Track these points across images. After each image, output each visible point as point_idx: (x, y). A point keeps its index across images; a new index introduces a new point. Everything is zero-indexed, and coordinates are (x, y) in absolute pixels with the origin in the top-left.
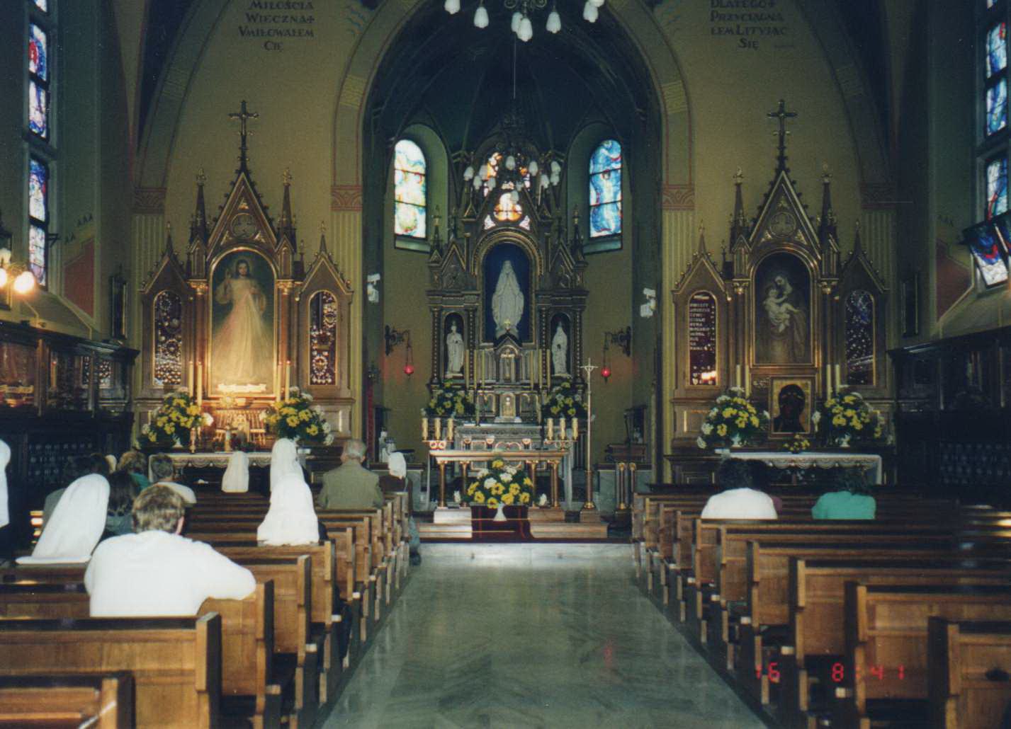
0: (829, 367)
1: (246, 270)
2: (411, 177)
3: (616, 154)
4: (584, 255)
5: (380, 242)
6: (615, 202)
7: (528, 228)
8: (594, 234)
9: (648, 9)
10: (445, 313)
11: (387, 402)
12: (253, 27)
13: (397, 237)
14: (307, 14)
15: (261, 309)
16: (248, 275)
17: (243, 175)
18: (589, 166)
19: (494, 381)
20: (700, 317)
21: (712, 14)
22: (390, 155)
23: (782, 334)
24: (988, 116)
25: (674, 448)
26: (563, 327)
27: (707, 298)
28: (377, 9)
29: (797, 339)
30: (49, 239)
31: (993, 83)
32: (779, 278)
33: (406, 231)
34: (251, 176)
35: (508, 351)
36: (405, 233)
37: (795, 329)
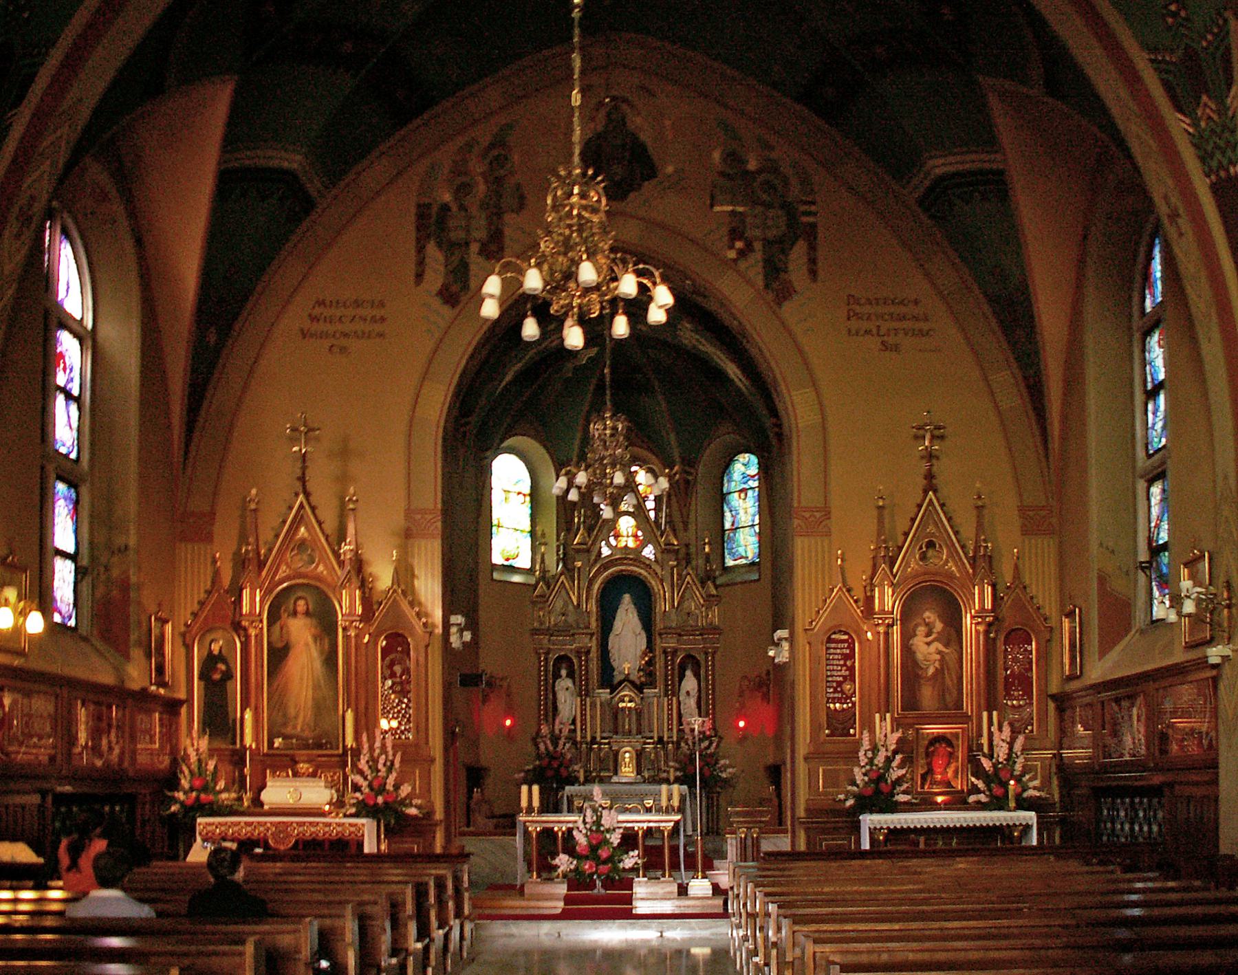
0: (985, 714)
1: (305, 608)
2: (513, 496)
3: (754, 470)
4: (716, 587)
5: (473, 577)
6: (753, 526)
7: (652, 557)
8: (730, 562)
9: (775, 307)
10: (553, 657)
11: (487, 756)
12: (321, 327)
13: (494, 567)
14: (378, 313)
15: (322, 653)
16: (307, 613)
17: (301, 497)
18: (722, 485)
19: (611, 735)
20: (839, 660)
21: (849, 315)
22: (484, 474)
23: (930, 679)
24: (1150, 431)
25: (807, 810)
26: (692, 670)
27: (846, 637)
28: (461, 305)
29: (948, 682)
30: (80, 573)
31: (1152, 394)
32: (927, 614)
33: (507, 560)
34: (311, 498)
35: (627, 699)
36: (506, 563)
37: (946, 672)
